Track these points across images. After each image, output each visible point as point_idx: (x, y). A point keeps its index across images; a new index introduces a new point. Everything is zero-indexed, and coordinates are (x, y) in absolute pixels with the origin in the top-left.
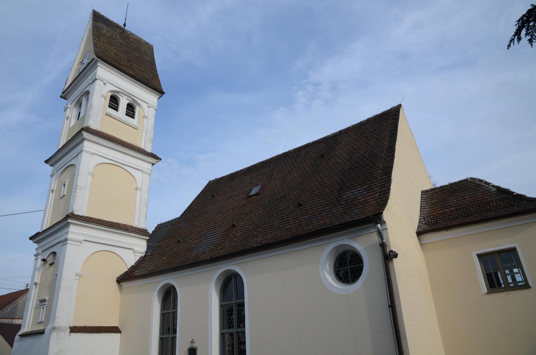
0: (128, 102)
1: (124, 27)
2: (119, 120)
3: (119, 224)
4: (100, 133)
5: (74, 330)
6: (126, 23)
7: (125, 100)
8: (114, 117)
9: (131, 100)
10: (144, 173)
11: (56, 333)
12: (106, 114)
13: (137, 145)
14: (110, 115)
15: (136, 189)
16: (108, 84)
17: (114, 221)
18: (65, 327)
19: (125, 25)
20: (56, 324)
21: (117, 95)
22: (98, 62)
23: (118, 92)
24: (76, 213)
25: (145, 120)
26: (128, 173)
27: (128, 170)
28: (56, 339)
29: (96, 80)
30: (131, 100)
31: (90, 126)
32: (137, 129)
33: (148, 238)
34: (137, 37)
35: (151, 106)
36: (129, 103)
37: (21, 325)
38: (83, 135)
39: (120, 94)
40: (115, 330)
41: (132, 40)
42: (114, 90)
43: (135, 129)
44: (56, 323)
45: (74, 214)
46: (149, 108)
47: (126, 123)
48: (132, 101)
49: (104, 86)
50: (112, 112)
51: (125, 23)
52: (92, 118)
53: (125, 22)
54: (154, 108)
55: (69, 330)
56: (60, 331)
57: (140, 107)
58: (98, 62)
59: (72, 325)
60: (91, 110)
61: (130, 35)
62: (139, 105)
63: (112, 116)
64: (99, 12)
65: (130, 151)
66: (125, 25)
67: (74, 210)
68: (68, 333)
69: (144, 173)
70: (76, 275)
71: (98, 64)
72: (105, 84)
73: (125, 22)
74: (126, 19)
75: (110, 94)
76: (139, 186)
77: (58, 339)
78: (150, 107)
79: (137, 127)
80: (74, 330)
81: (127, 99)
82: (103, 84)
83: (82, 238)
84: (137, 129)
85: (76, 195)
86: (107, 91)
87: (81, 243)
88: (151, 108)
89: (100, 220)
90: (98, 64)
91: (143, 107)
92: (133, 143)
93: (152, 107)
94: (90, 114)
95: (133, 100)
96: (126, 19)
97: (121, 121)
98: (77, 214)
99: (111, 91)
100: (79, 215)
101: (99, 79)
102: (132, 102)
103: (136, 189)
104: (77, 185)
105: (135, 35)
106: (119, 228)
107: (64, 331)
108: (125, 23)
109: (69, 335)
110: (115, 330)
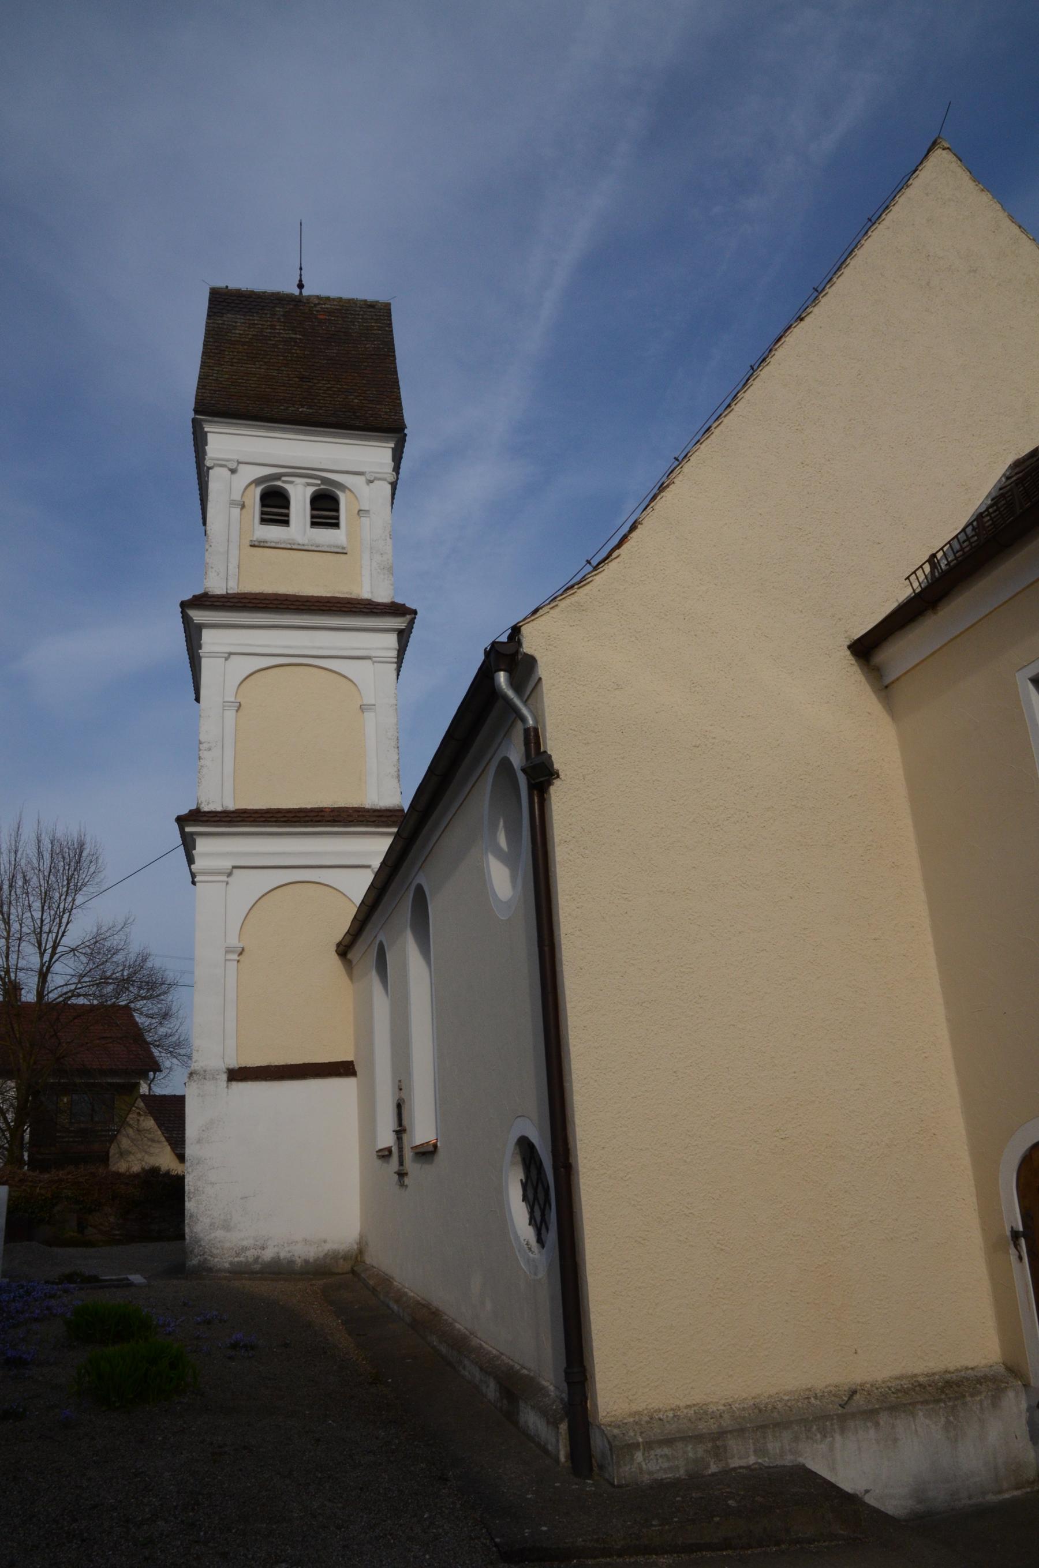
0: (310, 491)
1: (301, 293)
2: (289, 546)
3: (321, 810)
4: (359, 604)
5: (238, 1075)
6: (303, 279)
7: (300, 488)
8: (273, 545)
9: (319, 482)
10: (376, 662)
11: (196, 1083)
12: (251, 546)
13: (351, 594)
14: (262, 544)
15: (363, 708)
16: (242, 468)
17: (309, 806)
18: (217, 1070)
19: (301, 286)
20: (195, 1064)
21: (279, 483)
22: (203, 423)
23: (278, 477)
24: (206, 808)
25: (365, 521)
26: (335, 675)
27: (324, 666)
28: (198, 1096)
29: (210, 471)
30: (319, 482)
31: (210, 590)
32: (346, 553)
33: (395, 830)
34: (340, 299)
35: (372, 479)
36: (315, 492)
37: (185, 1096)
38: (192, 618)
39: (284, 479)
40: (344, 1069)
41: (324, 317)
42: (269, 475)
43: (339, 555)
44: (195, 1062)
45: (202, 810)
46: (371, 484)
47: (311, 548)
48: (322, 483)
49: (234, 476)
50: (273, 533)
51: (301, 281)
52: (212, 568)
53: (301, 275)
54: (384, 480)
55: (225, 1077)
56: (205, 1079)
57: (347, 491)
58: (203, 423)
59: (234, 1064)
60: (207, 550)
61: (316, 305)
62: (342, 487)
63: (268, 544)
64: (227, 287)
65: (317, 617)
66: (301, 286)
67: (200, 802)
68: (225, 1084)
69: (376, 662)
70: (227, 952)
71: (206, 429)
72: (233, 471)
73: (301, 275)
74: (301, 269)
75: (258, 491)
76: (369, 700)
77: (202, 1096)
78: (372, 482)
79: (343, 548)
80: (238, 1075)
81: (309, 484)
82: (229, 473)
83: (227, 864)
84: (346, 553)
85: (202, 766)
86: (243, 487)
87: (230, 875)
88: (376, 482)
89: (268, 811)
90: (206, 429)
91: (354, 491)
92: (339, 592)
93: (379, 479)
94: (208, 560)
95: (325, 481)
96: (301, 269)
97: (294, 547)
98: (210, 810)
99: (257, 482)
100: (214, 810)
101: (214, 464)
102: (322, 487)
103: (363, 708)
104: (200, 741)
105: (334, 299)
106: (312, 821)
107: (214, 1078)
108: (301, 281)
109: (227, 1087)
110: (344, 1069)
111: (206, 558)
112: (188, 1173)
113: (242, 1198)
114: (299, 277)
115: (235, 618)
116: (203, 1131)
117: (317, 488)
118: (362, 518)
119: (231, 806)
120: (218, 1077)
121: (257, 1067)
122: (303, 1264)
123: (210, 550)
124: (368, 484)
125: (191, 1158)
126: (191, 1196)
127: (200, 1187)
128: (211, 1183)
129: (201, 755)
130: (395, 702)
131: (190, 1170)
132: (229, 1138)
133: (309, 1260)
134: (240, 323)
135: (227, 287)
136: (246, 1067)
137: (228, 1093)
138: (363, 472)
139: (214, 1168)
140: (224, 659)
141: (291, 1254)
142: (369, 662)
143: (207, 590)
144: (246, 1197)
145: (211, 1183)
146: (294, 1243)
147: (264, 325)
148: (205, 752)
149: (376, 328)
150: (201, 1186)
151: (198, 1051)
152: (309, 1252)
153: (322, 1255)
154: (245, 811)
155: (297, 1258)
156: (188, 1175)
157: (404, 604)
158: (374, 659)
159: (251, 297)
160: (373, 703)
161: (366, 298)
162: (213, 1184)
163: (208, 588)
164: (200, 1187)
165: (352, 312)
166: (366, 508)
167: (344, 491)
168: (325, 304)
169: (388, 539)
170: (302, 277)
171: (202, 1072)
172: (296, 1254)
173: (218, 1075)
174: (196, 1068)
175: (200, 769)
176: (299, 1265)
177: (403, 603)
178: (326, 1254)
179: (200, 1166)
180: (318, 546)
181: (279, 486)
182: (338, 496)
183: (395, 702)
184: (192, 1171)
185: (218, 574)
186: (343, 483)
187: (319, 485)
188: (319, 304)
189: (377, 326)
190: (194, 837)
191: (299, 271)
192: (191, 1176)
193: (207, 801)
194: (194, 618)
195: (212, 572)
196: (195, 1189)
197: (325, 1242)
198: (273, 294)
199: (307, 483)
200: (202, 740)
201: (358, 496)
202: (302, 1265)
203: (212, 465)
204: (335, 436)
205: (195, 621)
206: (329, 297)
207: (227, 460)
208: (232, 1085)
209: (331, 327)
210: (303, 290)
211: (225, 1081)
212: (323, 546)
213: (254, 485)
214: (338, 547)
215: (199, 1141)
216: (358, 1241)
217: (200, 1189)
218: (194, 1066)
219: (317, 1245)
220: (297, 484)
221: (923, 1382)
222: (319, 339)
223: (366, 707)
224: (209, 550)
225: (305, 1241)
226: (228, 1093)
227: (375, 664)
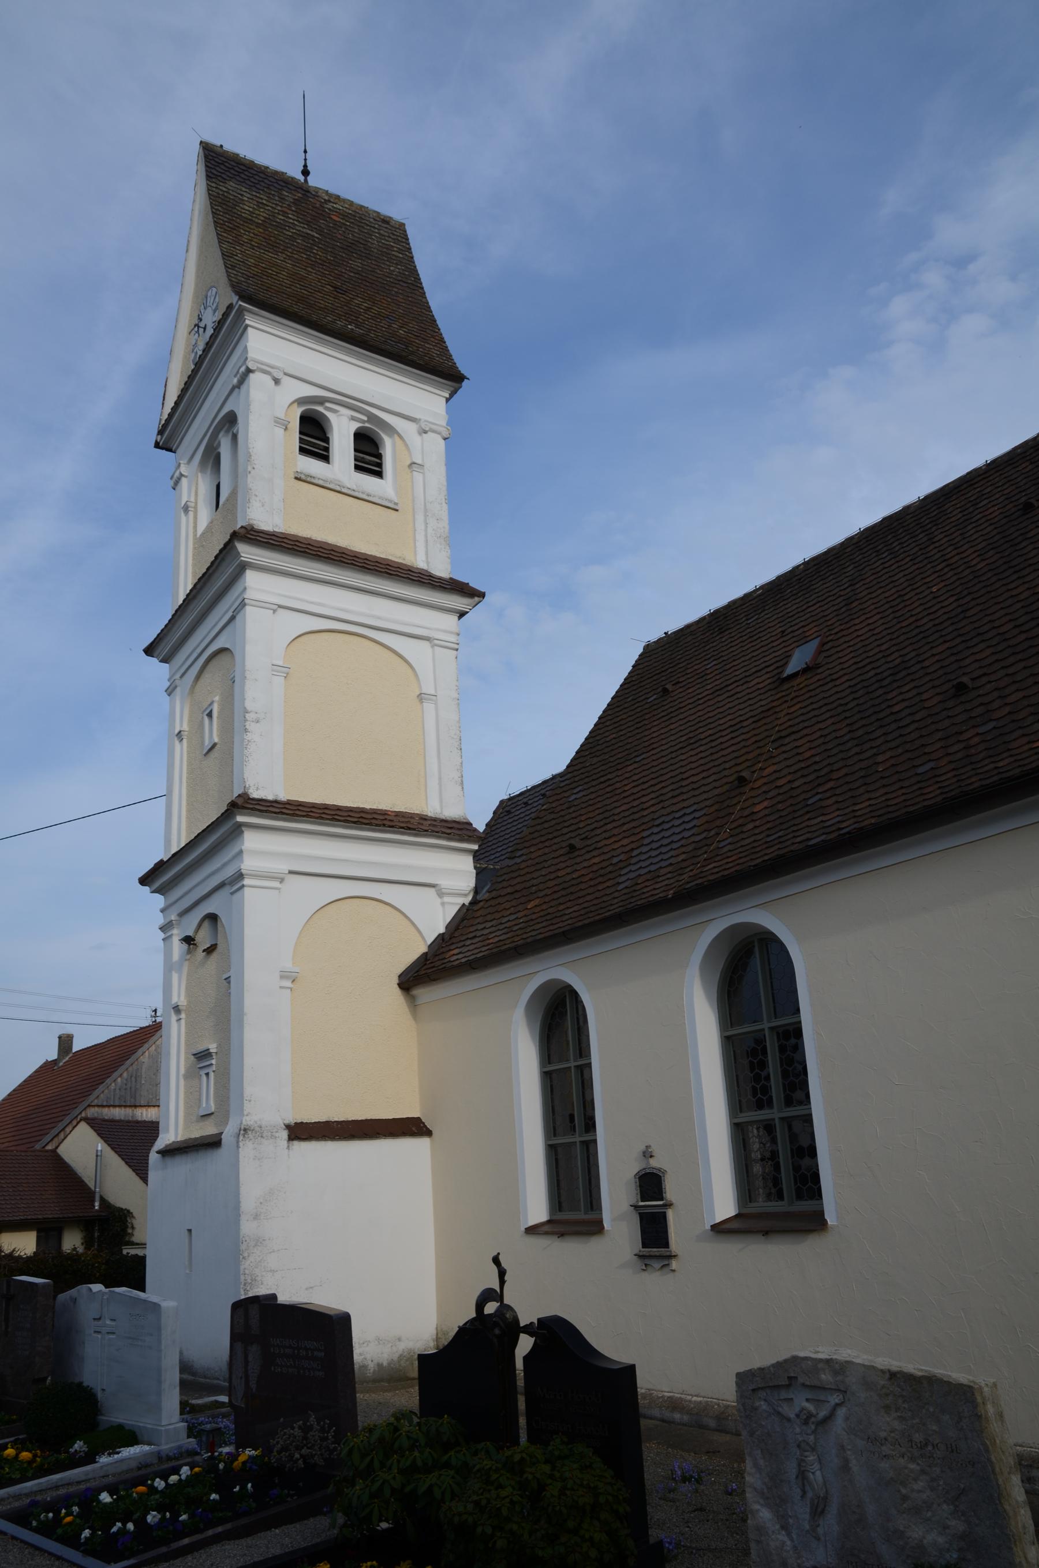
0: (354, 426)
1: (306, 180)
2: (338, 488)
7: (345, 420)
8: (321, 482)
9: (365, 418)
11: (251, 1142)
12: (296, 478)
14: (309, 479)
19: (306, 172)
20: (248, 1118)
21: (320, 409)
22: (246, 313)
23: (321, 401)
24: (255, 794)
25: (418, 477)
29: (251, 375)
30: (365, 418)
31: (255, 522)
32: (397, 510)
35: (427, 429)
38: (239, 553)
39: (328, 405)
44: (247, 1115)
45: (252, 796)
46: (424, 435)
48: (368, 421)
49: (278, 388)
50: (312, 466)
51: (305, 166)
53: (305, 160)
54: (439, 433)
55: (284, 1134)
56: (262, 1137)
57: (396, 436)
58: (246, 313)
60: (250, 472)
61: (327, 201)
63: (313, 480)
64: (221, 146)
66: (306, 172)
67: (247, 786)
68: (285, 1143)
73: (305, 160)
74: (305, 152)
76: (428, 688)
77: (259, 1159)
78: (426, 432)
79: (396, 504)
81: (353, 418)
82: (273, 383)
84: (397, 510)
86: (288, 405)
90: (247, 322)
94: (250, 485)
95: (372, 418)
96: (305, 152)
97: (343, 490)
99: (301, 401)
100: (264, 798)
102: (367, 425)
103: (421, 697)
106: (384, 825)
108: (305, 166)
111: (249, 482)
112: (243, 1258)
113: (307, 1289)
114: (303, 161)
115: (269, 559)
116: (261, 1203)
117: (361, 425)
118: (415, 473)
119: (283, 796)
120: (277, 1135)
121: (315, 1123)
122: (377, 1369)
123: (253, 472)
124: (420, 434)
125: (247, 1238)
126: (248, 1288)
127: (257, 1276)
128: (271, 1271)
129: (247, 727)
130: (456, 695)
131: (246, 1254)
132: (292, 1212)
133: (382, 1364)
134: (248, 198)
135: (221, 146)
136: (302, 1123)
137: (289, 1155)
138: (416, 419)
139: (274, 1252)
140: (272, 611)
141: (363, 1357)
142: (425, 644)
143: (251, 522)
144: (311, 1288)
145: (271, 1271)
146: (366, 1344)
147: (275, 209)
148: (253, 724)
149: (395, 249)
150: (259, 1275)
151: (250, 1101)
152: (382, 1353)
153: (395, 1357)
154: (300, 805)
155: (370, 1362)
156: (244, 1260)
157: (468, 584)
158: (436, 642)
159: (252, 169)
160: (433, 692)
161: (391, 216)
162: (273, 1271)
163: (252, 519)
164: (257, 1276)
165: (367, 223)
166: (419, 462)
167: (390, 436)
168: (336, 204)
169: (444, 504)
170: (307, 161)
171: (257, 1129)
172: (368, 1357)
173: (277, 1132)
174: (249, 1123)
175: (247, 745)
176: (372, 1371)
177: (466, 582)
178: (401, 1355)
179: (257, 1250)
180: (368, 495)
181: (321, 413)
182: (382, 439)
183: (456, 695)
184: (248, 1256)
185: (263, 506)
186: (393, 425)
187: (363, 422)
188: (329, 201)
189: (397, 248)
190: (243, 829)
191: (304, 154)
192: (248, 1262)
193: (256, 786)
194: (242, 555)
195: (256, 501)
196: (252, 1280)
197: (399, 1340)
198: (276, 173)
199: (352, 416)
200: (249, 708)
201: (408, 442)
202: (374, 1371)
203: (255, 368)
204: (389, 368)
205: (242, 558)
206: (339, 196)
207: (272, 367)
208: (293, 1145)
209: (349, 234)
210: (309, 178)
211: (285, 1140)
212: (374, 496)
213: (296, 404)
214: (390, 501)
215: (256, 1217)
216: (435, 1337)
217: (259, 1279)
218: (246, 1120)
219: (391, 1344)
220: (341, 415)
221: (1020, 1452)
222: (338, 244)
223: (426, 696)
224: (252, 472)
225: (378, 1340)
226: (289, 1155)
227: (436, 648)
